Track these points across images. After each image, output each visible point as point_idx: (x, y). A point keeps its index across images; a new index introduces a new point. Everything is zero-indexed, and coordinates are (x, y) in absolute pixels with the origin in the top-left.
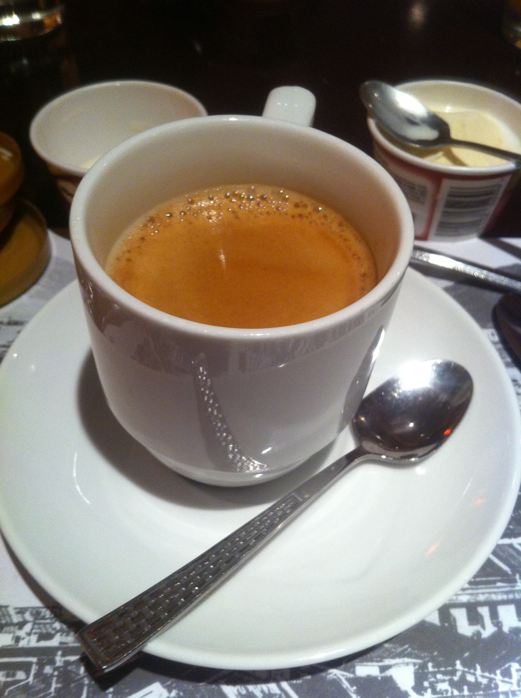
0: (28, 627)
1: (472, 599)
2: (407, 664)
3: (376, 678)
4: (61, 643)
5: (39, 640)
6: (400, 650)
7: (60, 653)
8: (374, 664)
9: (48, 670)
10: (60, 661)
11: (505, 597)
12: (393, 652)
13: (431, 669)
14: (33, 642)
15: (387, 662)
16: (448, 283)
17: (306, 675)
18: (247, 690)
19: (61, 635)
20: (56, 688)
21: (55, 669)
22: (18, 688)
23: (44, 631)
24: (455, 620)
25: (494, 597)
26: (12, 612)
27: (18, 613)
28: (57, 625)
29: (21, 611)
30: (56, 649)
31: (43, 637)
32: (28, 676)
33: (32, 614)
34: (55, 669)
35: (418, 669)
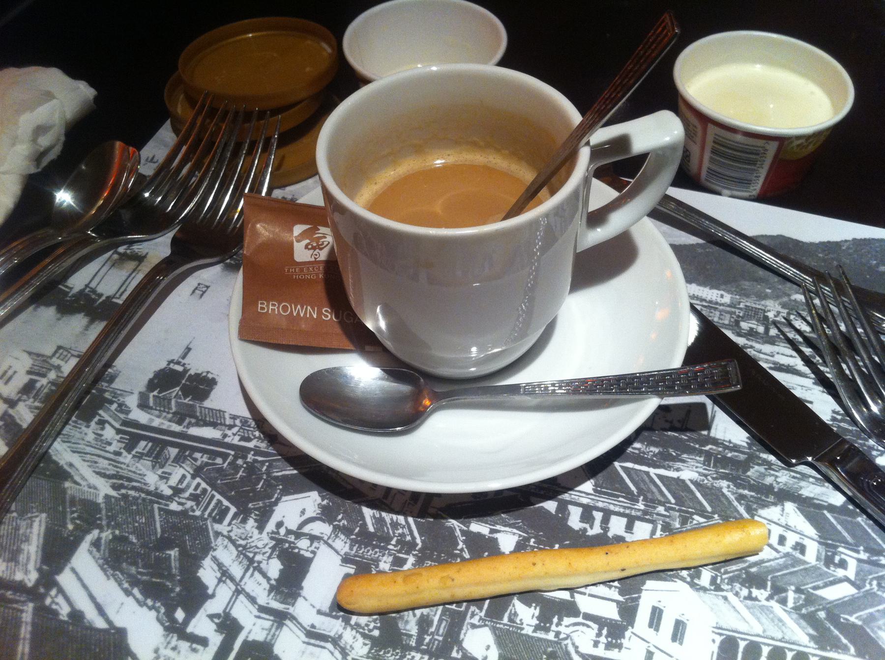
0: (235, 430)
1: (591, 503)
2: (514, 534)
3: (484, 536)
4: (255, 446)
5: (240, 440)
6: (512, 522)
7: (252, 453)
8: (488, 526)
9: (240, 462)
10: (251, 458)
11: (622, 510)
12: (506, 522)
13: (532, 543)
14: (236, 441)
15: (498, 527)
16: (8, 262)
17: (429, 518)
18: (381, 515)
19: (258, 441)
20: (241, 475)
21: (245, 463)
22: (213, 469)
23: (246, 435)
24: (569, 514)
25: (612, 507)
26: (227, 416)
27: (230, 418)
28: (257, 433)
29: (234, 417)
30: (251, 449)
31: (243, 439)
32: (224, 463)
33: (241, 421)
34: (245, 463)
35: (522, 540)
